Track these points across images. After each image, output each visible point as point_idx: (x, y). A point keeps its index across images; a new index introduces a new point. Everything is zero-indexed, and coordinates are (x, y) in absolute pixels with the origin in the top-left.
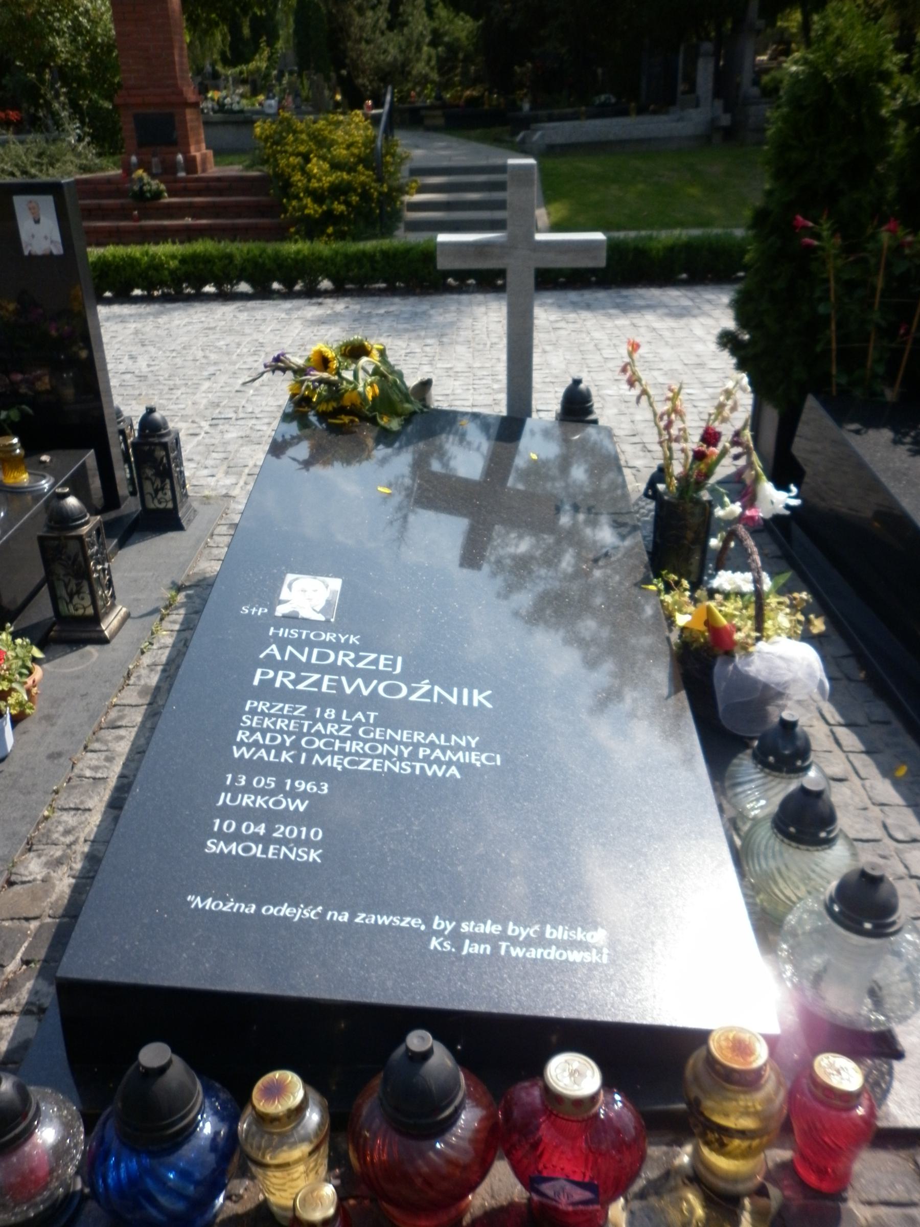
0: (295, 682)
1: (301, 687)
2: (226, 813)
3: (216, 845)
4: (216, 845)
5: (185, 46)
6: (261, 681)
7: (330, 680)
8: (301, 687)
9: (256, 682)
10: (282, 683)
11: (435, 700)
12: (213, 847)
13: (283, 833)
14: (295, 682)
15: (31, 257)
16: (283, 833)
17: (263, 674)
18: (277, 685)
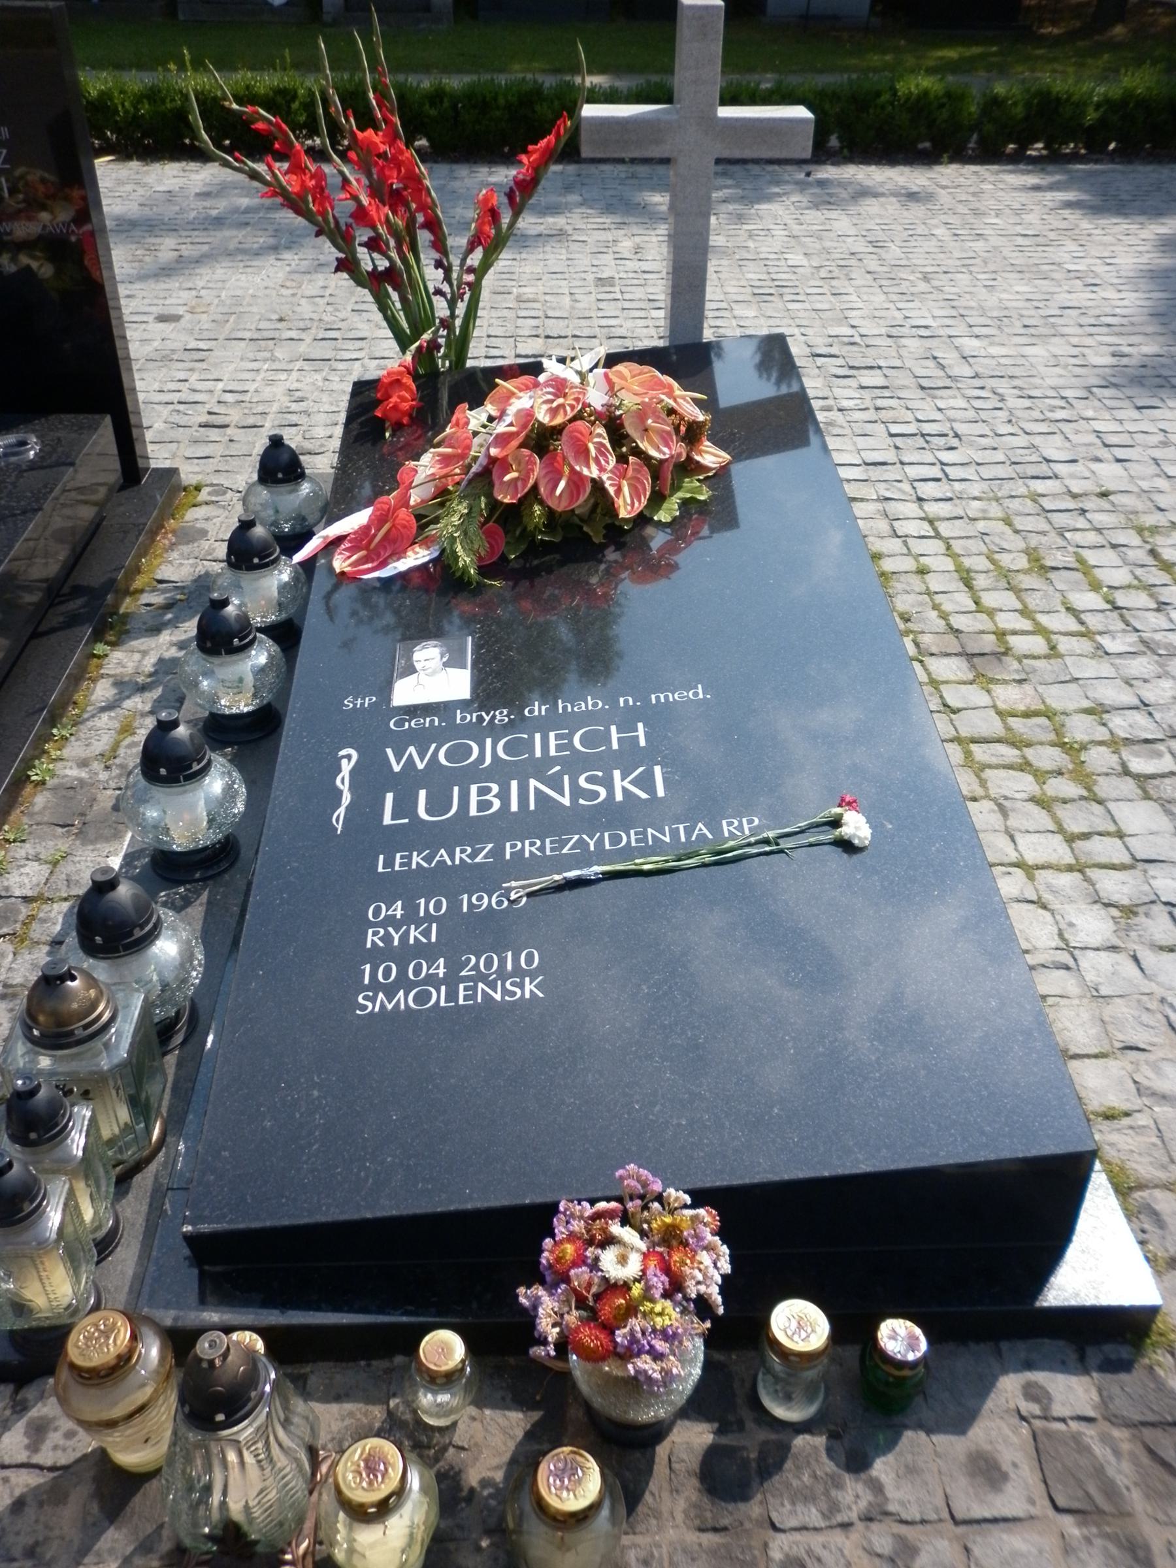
0: (472, 856)
1: (477, 860)
2: (376, 956)
3: (373, 1000)
4: (373, 1000)
5: (370, 415)
6: (511, 854)
7: (551, 842)
8: (477, 860)
9: (508, 857)
10: (461, 859)
11: (667, 828)
12: (369, 1005)
13: (476, 967)
14: (472, 856)
15: (708, 1419)
16: (476, 967)
17: (513, 846)
18: (527, 855)
